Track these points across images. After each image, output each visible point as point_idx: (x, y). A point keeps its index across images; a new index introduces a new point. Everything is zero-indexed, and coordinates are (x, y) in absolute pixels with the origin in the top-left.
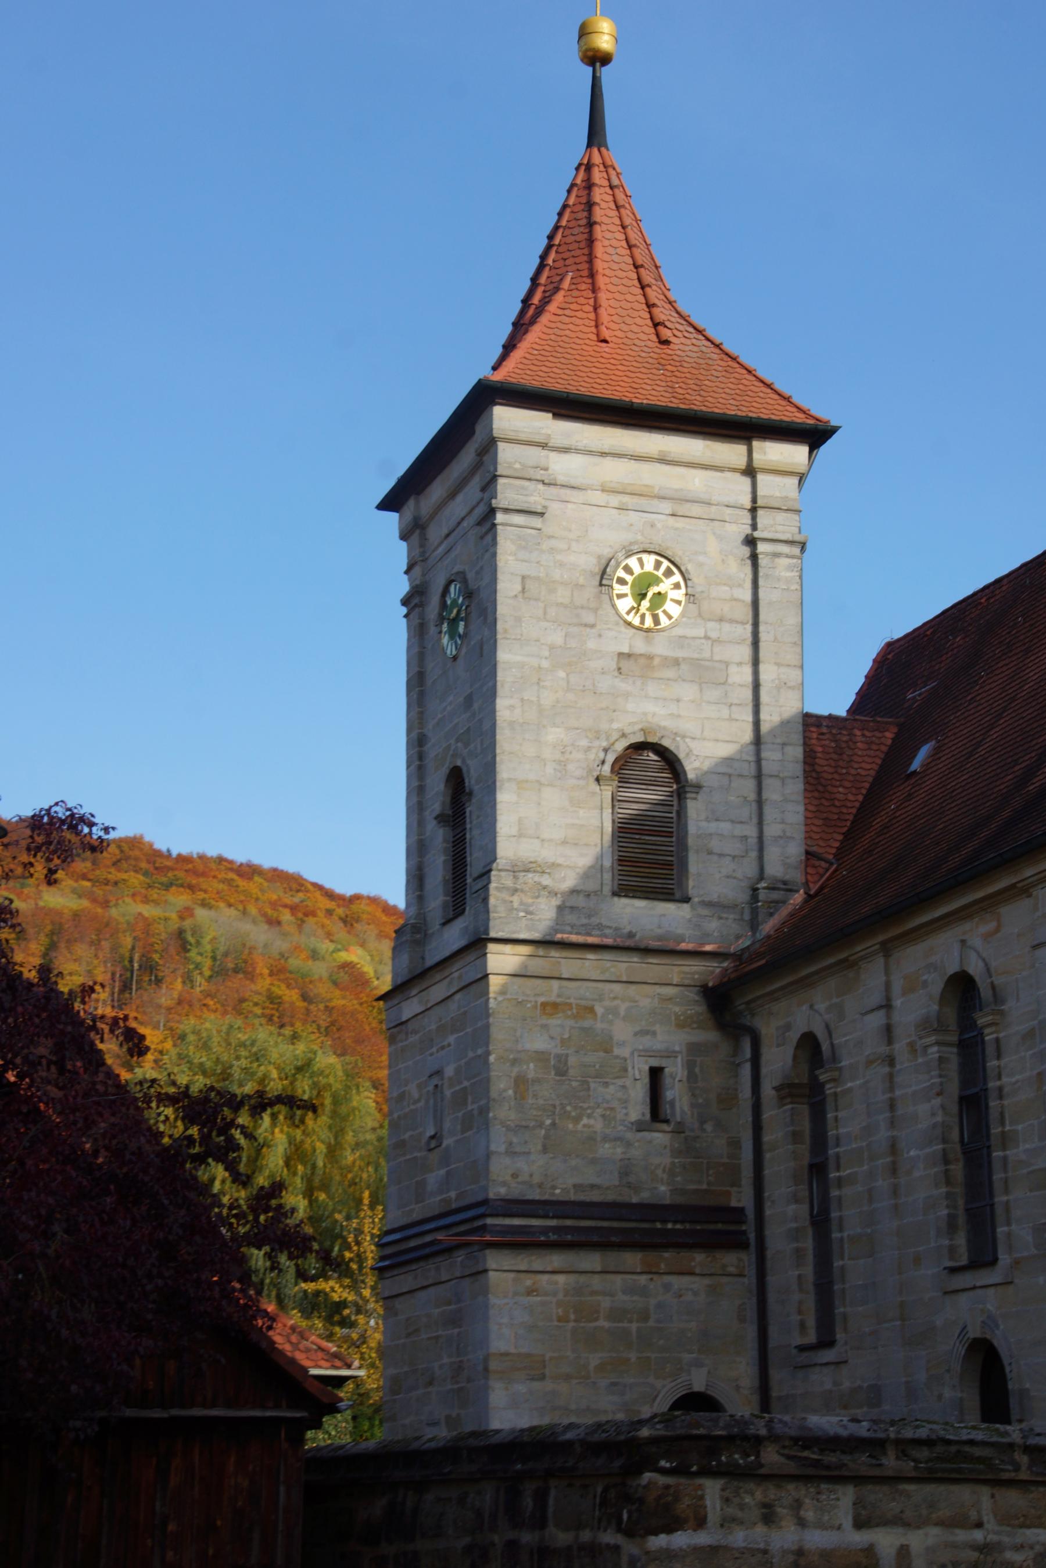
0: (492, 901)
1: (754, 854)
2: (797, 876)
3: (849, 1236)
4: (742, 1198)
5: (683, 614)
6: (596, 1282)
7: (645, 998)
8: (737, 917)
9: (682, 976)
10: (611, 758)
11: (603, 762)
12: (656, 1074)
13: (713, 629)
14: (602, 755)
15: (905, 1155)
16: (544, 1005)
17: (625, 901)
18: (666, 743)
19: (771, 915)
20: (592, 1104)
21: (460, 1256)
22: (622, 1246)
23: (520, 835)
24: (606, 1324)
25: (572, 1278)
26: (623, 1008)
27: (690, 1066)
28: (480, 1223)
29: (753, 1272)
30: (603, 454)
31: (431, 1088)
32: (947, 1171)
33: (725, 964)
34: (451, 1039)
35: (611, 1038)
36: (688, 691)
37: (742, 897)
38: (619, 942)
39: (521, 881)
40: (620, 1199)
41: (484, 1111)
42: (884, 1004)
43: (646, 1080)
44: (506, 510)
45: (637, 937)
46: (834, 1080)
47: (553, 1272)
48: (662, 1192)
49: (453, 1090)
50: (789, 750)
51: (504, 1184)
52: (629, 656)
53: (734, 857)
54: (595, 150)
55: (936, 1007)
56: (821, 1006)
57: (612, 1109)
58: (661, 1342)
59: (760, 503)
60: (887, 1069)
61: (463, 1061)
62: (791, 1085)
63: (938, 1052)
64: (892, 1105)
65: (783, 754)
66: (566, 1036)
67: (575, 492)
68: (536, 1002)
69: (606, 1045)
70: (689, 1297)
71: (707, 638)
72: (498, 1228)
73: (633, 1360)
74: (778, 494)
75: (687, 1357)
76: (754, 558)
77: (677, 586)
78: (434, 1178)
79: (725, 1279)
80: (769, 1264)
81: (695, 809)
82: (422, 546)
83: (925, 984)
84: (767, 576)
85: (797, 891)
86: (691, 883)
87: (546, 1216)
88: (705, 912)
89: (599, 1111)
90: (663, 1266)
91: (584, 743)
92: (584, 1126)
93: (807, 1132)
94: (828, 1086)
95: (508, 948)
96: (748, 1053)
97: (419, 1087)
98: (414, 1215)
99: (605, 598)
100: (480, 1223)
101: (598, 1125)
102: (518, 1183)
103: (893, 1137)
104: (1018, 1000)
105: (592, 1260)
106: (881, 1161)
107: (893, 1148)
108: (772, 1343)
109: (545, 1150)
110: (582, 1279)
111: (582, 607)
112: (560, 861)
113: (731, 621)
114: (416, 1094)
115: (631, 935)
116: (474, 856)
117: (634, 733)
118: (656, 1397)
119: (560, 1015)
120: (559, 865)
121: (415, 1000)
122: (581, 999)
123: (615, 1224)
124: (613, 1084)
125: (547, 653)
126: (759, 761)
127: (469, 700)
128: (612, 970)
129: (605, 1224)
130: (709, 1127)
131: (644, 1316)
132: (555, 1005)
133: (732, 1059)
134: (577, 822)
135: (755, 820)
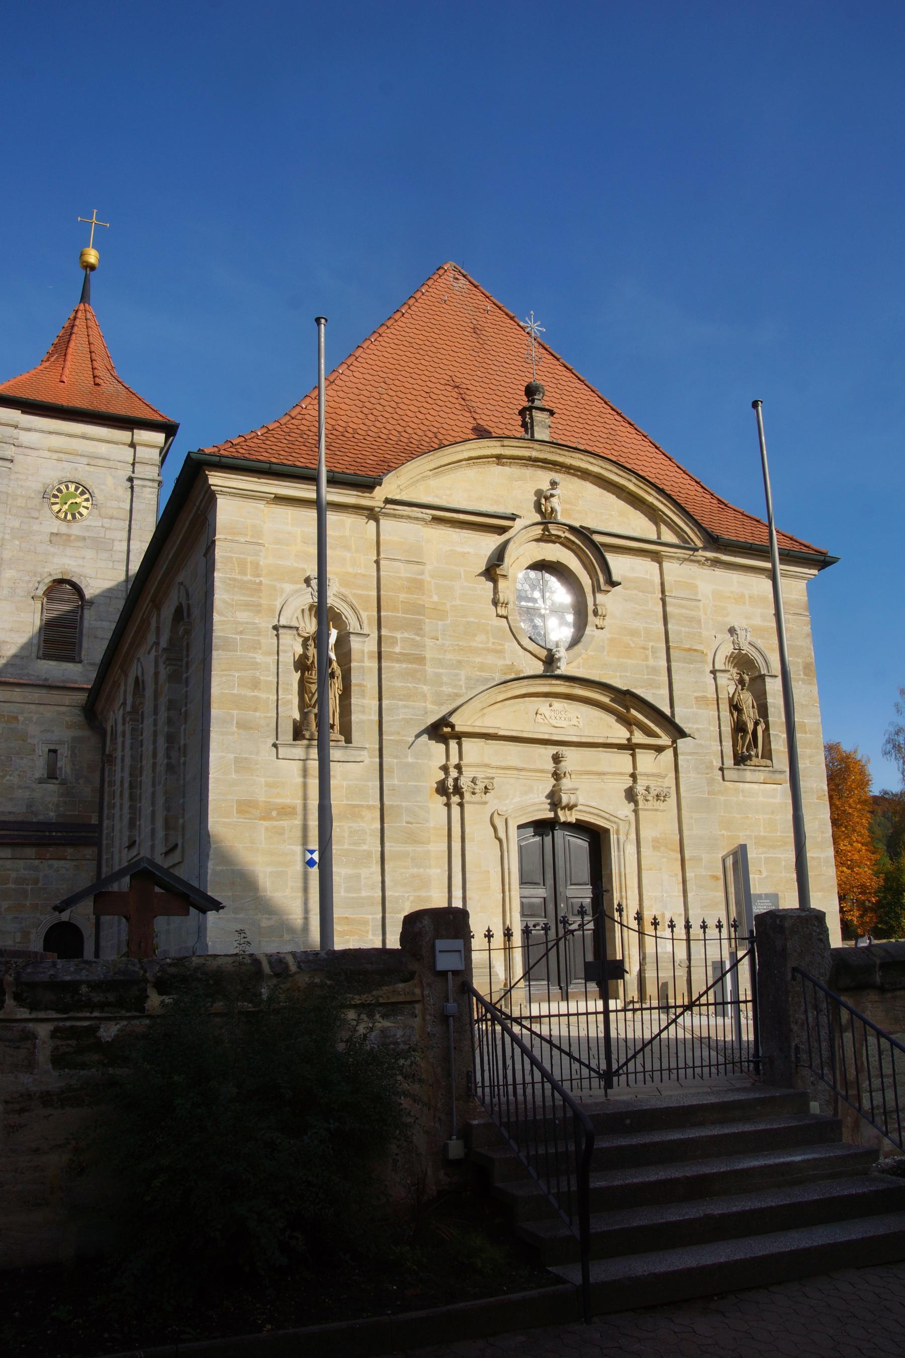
5: (89, 514)
6: (8, 864)
13: (107, 522)
14: (37, 585)
18: (74, 579)
22: (22, 845)
24: (13, 886)
26: (35, 717)
30: (50, 433)
36: (90, 554)
38: (41, 683)
45: (50, 681)
54: (82, 305)
59: (137, 460)
61: (687, 629)
67: (32, 451)
71: (103, 527)
74: (147, 457)
76: (132, 488)
77: (87, 500)
79: (84, 862)
81: (89, 615)
84: (138, 497)
86: (83, 653)
90: (48, 855)
91: (27, 578)
92: (7, 780)
99: (46, 505)
111: (32, 509)
112: (8, 640)
113: (117, 519)
115: (46, 680)
120: (7, 642)
130: (81, 781)
131: (36, 881)
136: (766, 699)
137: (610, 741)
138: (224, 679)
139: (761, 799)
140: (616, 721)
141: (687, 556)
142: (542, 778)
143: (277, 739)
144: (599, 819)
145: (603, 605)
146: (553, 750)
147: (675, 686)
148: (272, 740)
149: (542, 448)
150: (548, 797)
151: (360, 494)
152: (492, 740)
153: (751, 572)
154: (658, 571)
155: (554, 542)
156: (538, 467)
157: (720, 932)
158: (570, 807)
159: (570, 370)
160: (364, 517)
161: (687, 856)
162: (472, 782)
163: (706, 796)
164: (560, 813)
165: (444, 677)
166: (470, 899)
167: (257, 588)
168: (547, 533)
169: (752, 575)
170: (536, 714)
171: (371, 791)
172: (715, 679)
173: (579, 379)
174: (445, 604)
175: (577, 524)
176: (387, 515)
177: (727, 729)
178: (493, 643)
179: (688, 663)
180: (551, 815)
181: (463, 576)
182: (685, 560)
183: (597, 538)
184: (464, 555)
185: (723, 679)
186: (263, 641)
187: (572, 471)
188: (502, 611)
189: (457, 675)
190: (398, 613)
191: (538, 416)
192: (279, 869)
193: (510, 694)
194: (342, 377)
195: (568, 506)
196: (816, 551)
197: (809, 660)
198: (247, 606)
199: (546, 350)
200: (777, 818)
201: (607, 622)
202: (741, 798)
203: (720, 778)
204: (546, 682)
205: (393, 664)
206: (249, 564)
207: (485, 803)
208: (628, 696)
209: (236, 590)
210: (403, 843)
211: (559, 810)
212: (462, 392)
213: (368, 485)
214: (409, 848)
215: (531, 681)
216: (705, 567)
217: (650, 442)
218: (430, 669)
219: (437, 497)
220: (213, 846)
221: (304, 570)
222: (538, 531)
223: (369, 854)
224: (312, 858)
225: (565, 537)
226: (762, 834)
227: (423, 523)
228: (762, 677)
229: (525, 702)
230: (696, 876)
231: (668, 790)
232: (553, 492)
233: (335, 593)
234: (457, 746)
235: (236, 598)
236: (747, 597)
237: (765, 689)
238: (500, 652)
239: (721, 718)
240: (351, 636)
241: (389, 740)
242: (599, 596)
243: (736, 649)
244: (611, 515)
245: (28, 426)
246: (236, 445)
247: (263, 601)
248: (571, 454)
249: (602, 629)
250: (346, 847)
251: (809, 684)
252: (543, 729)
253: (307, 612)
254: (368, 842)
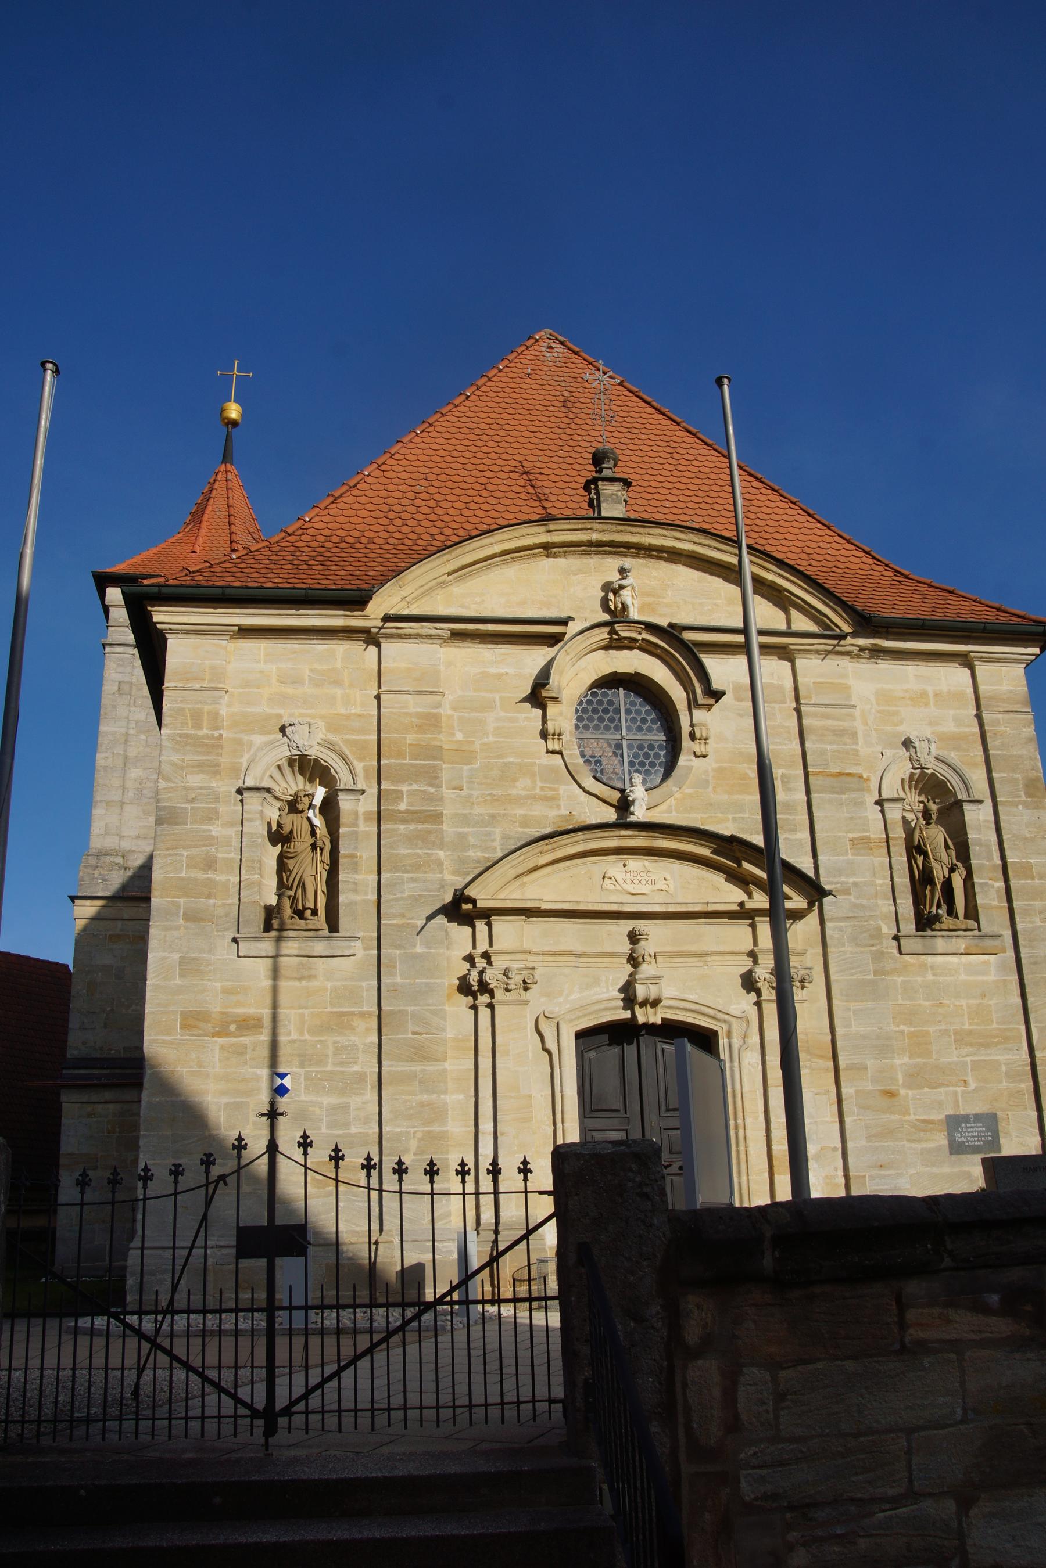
16: (111, 936)
23: (106, 834)
39: (101, 861)
44: (111, 645)
47: (106, 1102)
61: (835, 747)
95: (88, 902)
120: (134, 851)
125: (134, 726)
134: (146, 824)
136: (966, 834)
137: (712, 908)
138: (169, 860)
139: (963, 977)
140: (726, 880)
141: (830, 648)
142: (611, 965)
143: (491, 945)
144: (700, 1017)
145: (705, 725)
146: (627, 926)
147: (817, 827)
148: (231, 934)
149: (605, 527)
150: (622, 990)
151: (348, 613)
152: (537, 917)
153: (935, 661)
154: (790, 673)
155: (631, 648)
156: (605, 553)
157: (463, 1181)
158: (655, 1003)
159: (694, 434)
160: (361, 643)
161: (842, 1064)
162: (504, 974)
163: (872, 977)
164: (639, 1011)
165: (470, 838)
166: (502, 1135)
167: (215, 744)
168: (615, 637)
169: (938, 664)
170: (604, 878)
171: (365, 994)
172: (882, 812)
173: (706, 444)
174: (473, 742)
175: (664, 622)
177: (903, 881)
178: (542, 789)
179: (837, 793)
180: (627, 1015)
181: (498, 704)
182: (828, 653)
183: (689, 636)
184: (499, 676)
185: (894, 813)
186: (222, 809)
187: (655, 553)
188: (553, 745)
189: (489, 834)
190: (405, 760)
191: (606, 488)
192: (238, 1100)
193: (559, 854)
194: (369, 480)
195: (651, 600)
196: (1035, 621)
197: (1033, 774)
198: (201, 766)
199: (663, 414)
200: (991, 1002)
201: (711, 748)
202: (930, 977)
203: (895, 951)
204: (612, 834)
205: (397, 826)
206: (205, 714)
207: (526, 1003)
208: (735, 844)
209: (188, 748)
210: (407, 1061)
211: (637, 1008)
212: (532, 478)
213: (358, 601)
214: (417, 1068)
215: (589, 834)
216: (862, 660)
217: (801, 509)
218: (449, 829)
219: (462, 606)
220: (148, 1072)
221: (280, 716)
222: (603, 634)
223: (361, 1077)
224: (282, 1084)
225: (643, 639)
226: (966, 1027)
227: (440, 641)
228: (958, 804)
229: (586, 863)
230: (857, 1092)
231: (808, 972)
232: (624, 582)
233: (320, 741)
234: (486, 928)
235: (187, 758)
236: (931, 695)
237: (964, 821)
238: (551, 800)
239: (894, 867)
240: (340, 793)
241: (390, 925)
242: (699, 715)
243: (917, 769)
244: (716, 605)
246: (194, 572)
247: (225, 760)
248: (647, 530)
249: (705, 756)
250: (329, 1068)
251: (1035, 808)
252: (613, 898)
253: (287, 770)
254: (360, 1061)
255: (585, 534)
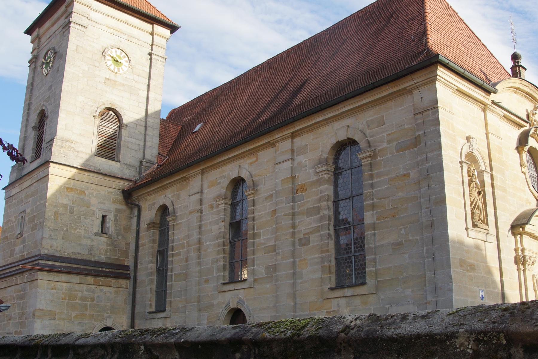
0: (53, 149)
1: (142, 151)
2: (155, 160)
3: (175, 274)
4: (129, 262)
6: (77, 287)
7: (103, 191)
8: (135, 170)
9: (116, 185)
10: (99, 111)
11: (96, 111)
12: (104, 217)
14: (96, 109)
15: (204, 244)
16: (68, 188)
17: (99, 158)
19: (146, 170)
20: (81, 225)
21: (26, 275)
24: (79, 302)
25: (69, 285)
26: (95, 193)
27: (116, 216)
28: (37, 262)
29: (132, 287)
30: (108, 16)
31: (20, 217)
32: (224, 248)
33: (131, 184)
34: (31, 199)
35: (90, 203)
37: (137, 164)
40: (88, 259)
41: (41, 223)
42: (200, 191)
43: (101, 219)
44: (75, 23)
46: (174, 220)
48: (103, 258)
49: (29, 217)
50: (156, 120)
51: (47, 249)
52: (109, 79)
53: (135, 151)
55: (225, 191)
56: (170, 196)
57: (88, 227)
58: (98, 309)
59: (154, 43)
60: (199, 214)
62: (154, 223)
63: (224, 206)
64: (200, 227)
65: (154, 121)
66: (74, 200)
68: (65, 186)
69: (88, 205)
70: (108, 294)
71: (134, 80)
72: (43, 264)
73: (88, 315)
75: (106, 315)
76: (151, 59)
78: (17, 249)
79: (121, 289)
80: (138, 285)
81: (124, 132)
82: (38, 44)
83: (219, 183)
85: (155, 164)
86: (121, 156)
87: (61, 262)
88: (125, 166)
89: (83, 227)
90: (101, 283)
92: (78, 232)
93: (158, 240)
94: (170, 222)
96: (136, 214)
97: (15, 217)
98: (9, 262)
100: (37, 262)
101: (83, 232)
102: (52, 249)
103: (200, 238)
104: (265, 184)
105: (76, 279)
106: (193, 247)
107: (199, 242)
108: (136, 311)
109: (63, 239)
110: (72, 285)
111: (95, 60)
113: (142, 77)
114: (14, 220)
115: (99, 170)
116: (46, 138)
117: (108, 104)
118: (95, 327)
119: (73, 192)
120: (77, 142)
121: (17, 188)
122: (81, 188)
123: (85, 267)
124: (89, 219)
126: (146, 122)
127: (51, 87)
128: (93, 180)
129: (82, 267)
130: (120, 237)
131: (93, 300)
132: (71, 189)
133: (130, 216)
135: (143, 140)
168: (535, 133)
176: (490, 110)
240: (51, 164)
245: (96, 9)
255: (527, 84)
